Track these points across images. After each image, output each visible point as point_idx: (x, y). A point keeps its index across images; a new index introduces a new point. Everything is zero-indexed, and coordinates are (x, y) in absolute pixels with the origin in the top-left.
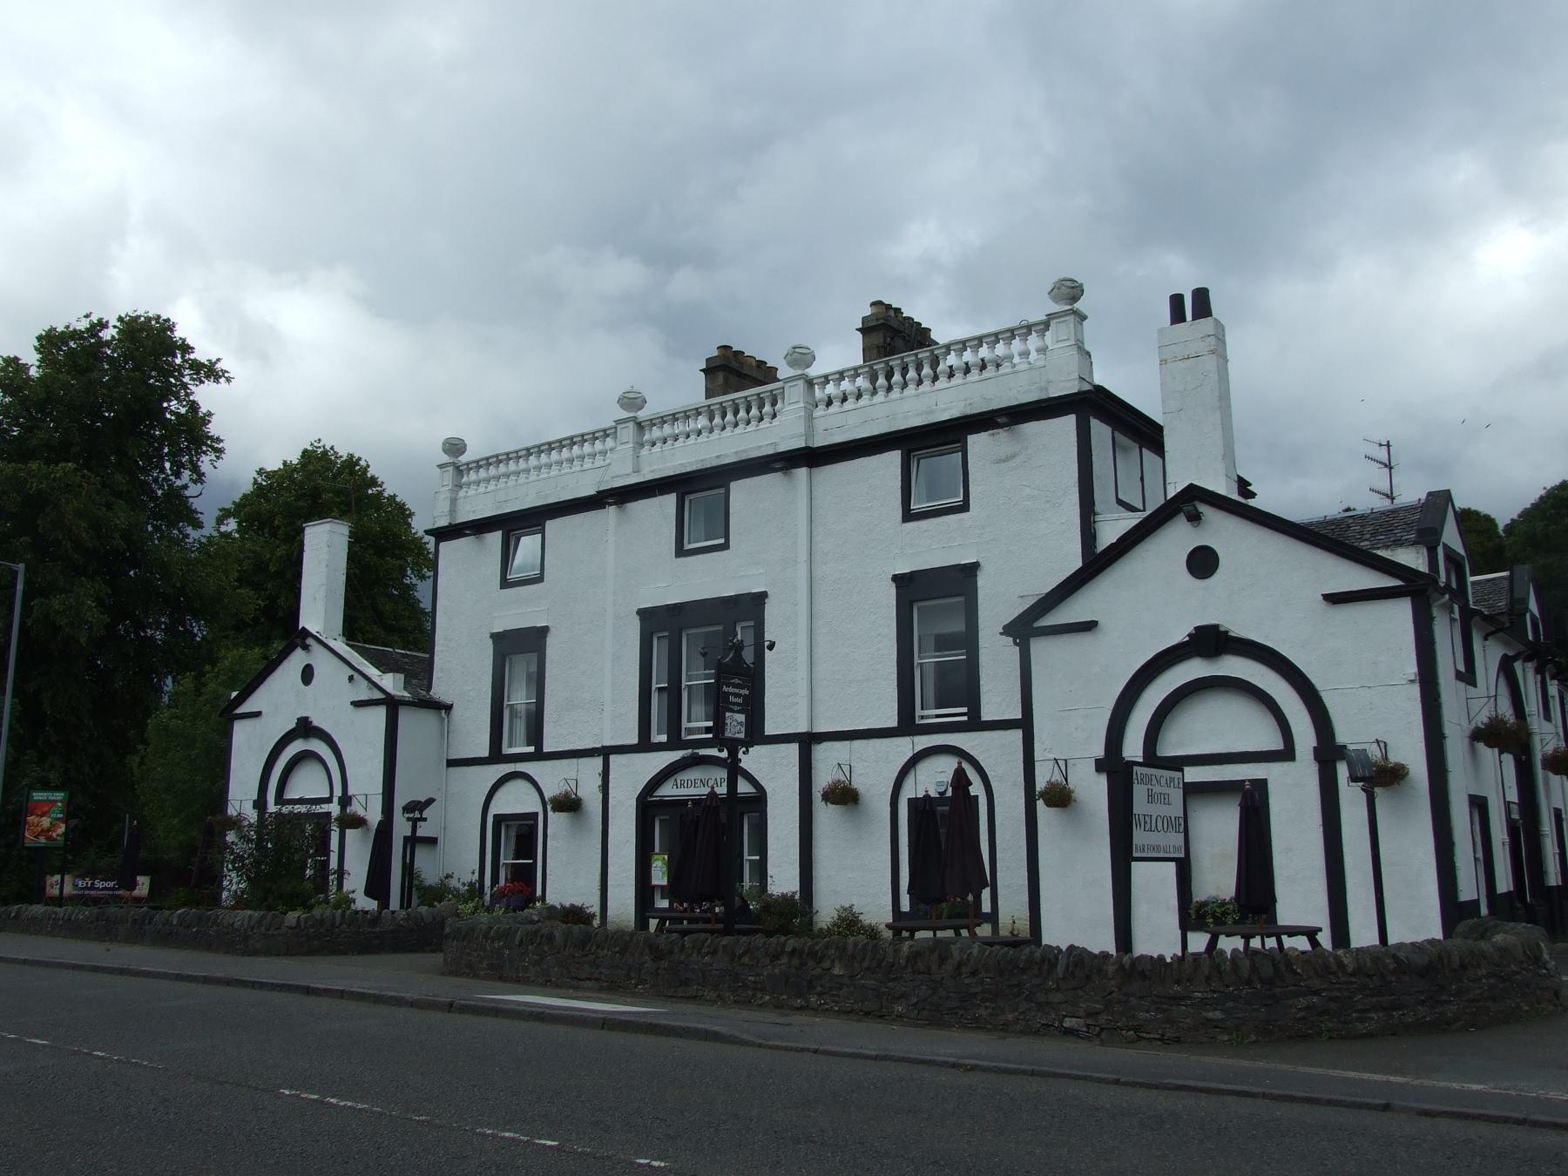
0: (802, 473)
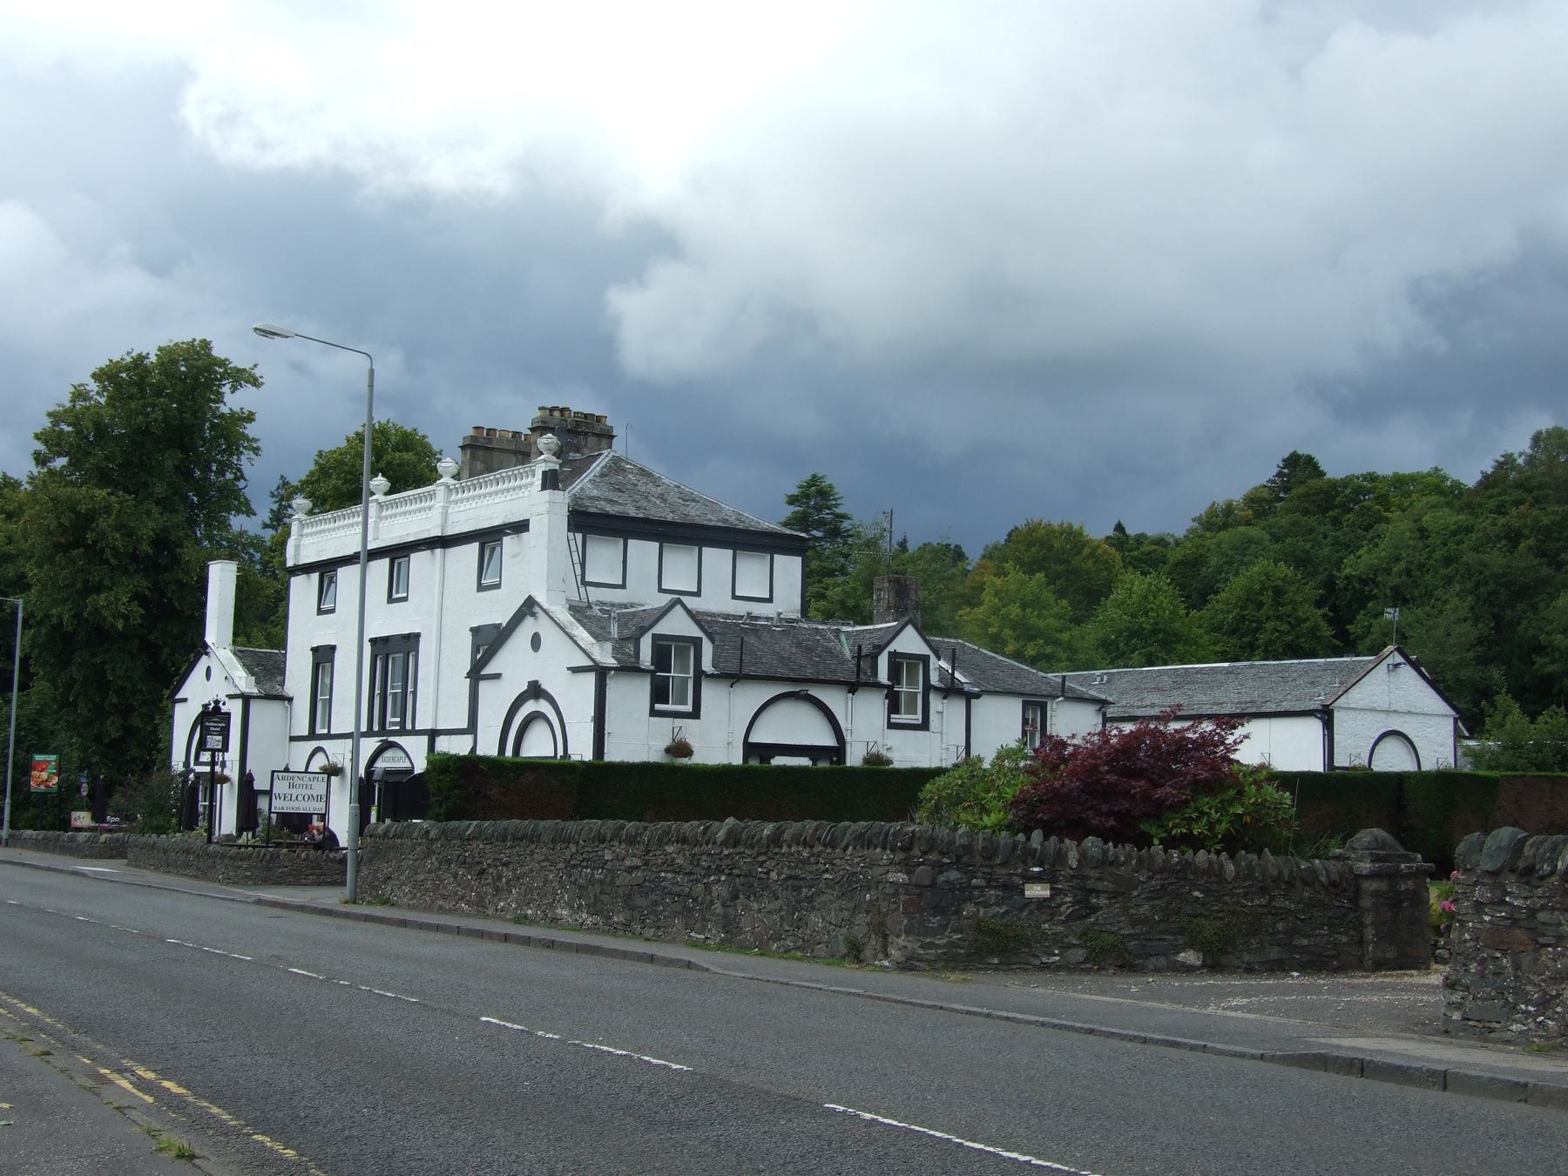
0: (438, 551)
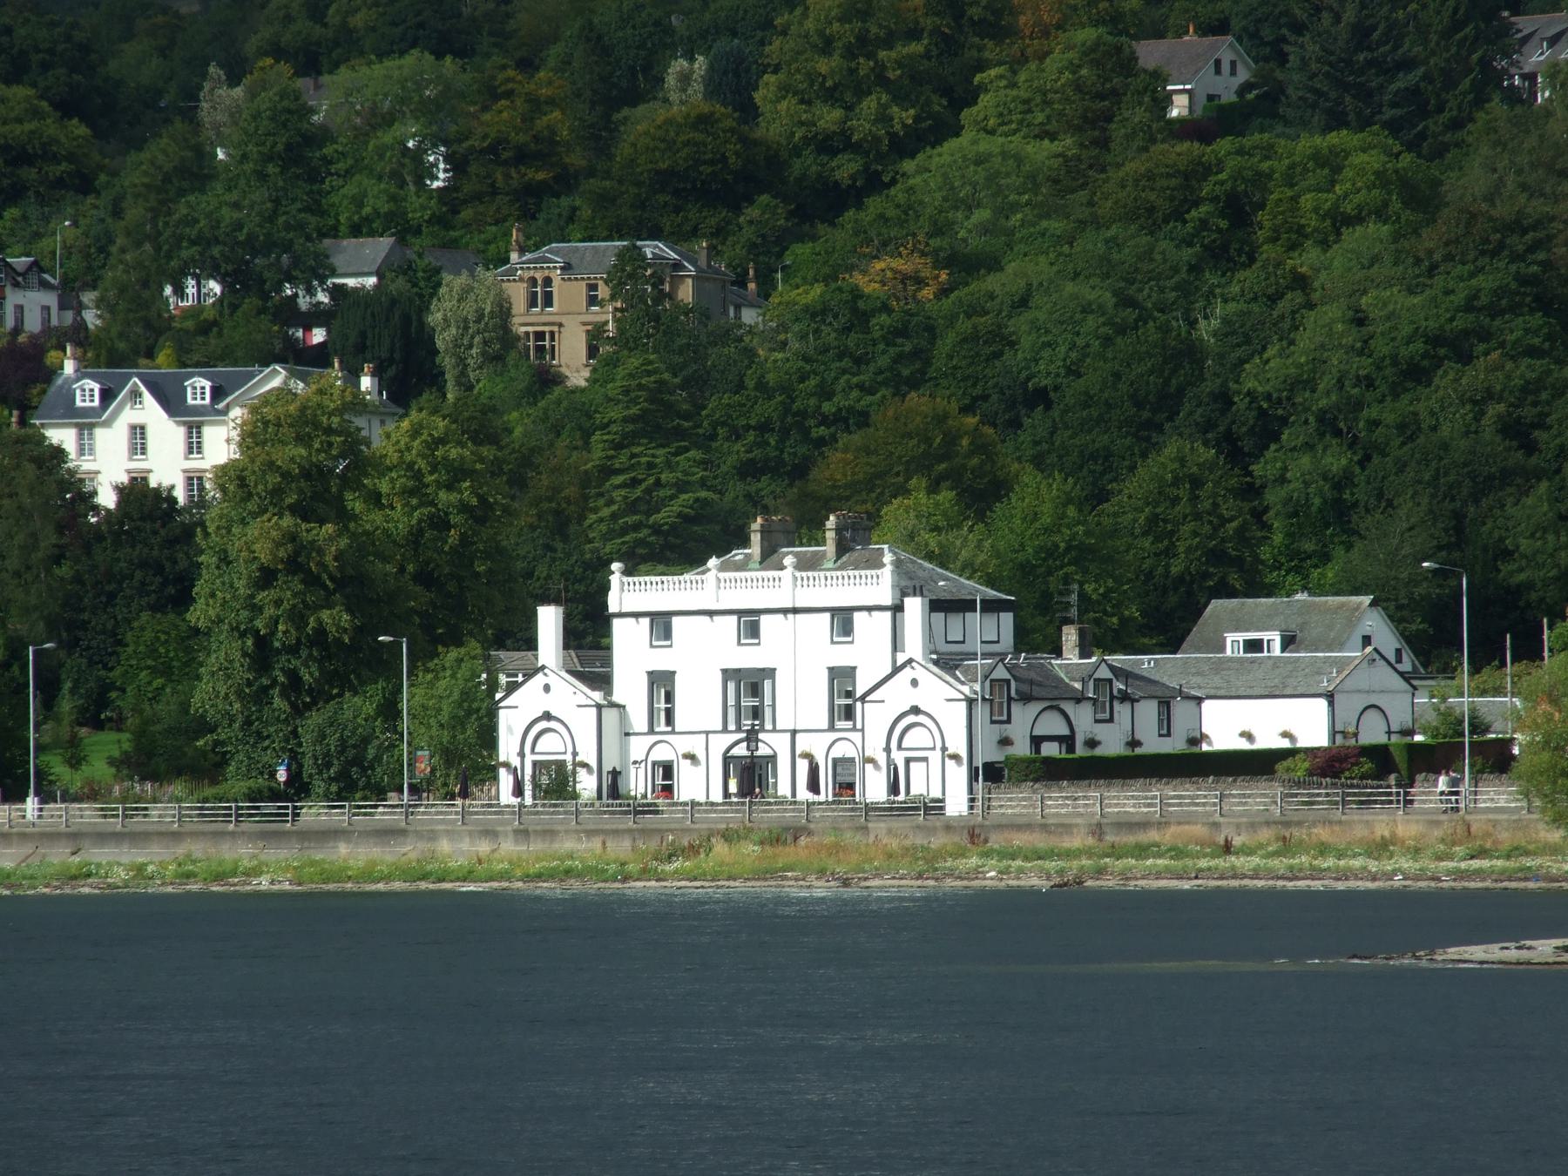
0: (790, 616)
